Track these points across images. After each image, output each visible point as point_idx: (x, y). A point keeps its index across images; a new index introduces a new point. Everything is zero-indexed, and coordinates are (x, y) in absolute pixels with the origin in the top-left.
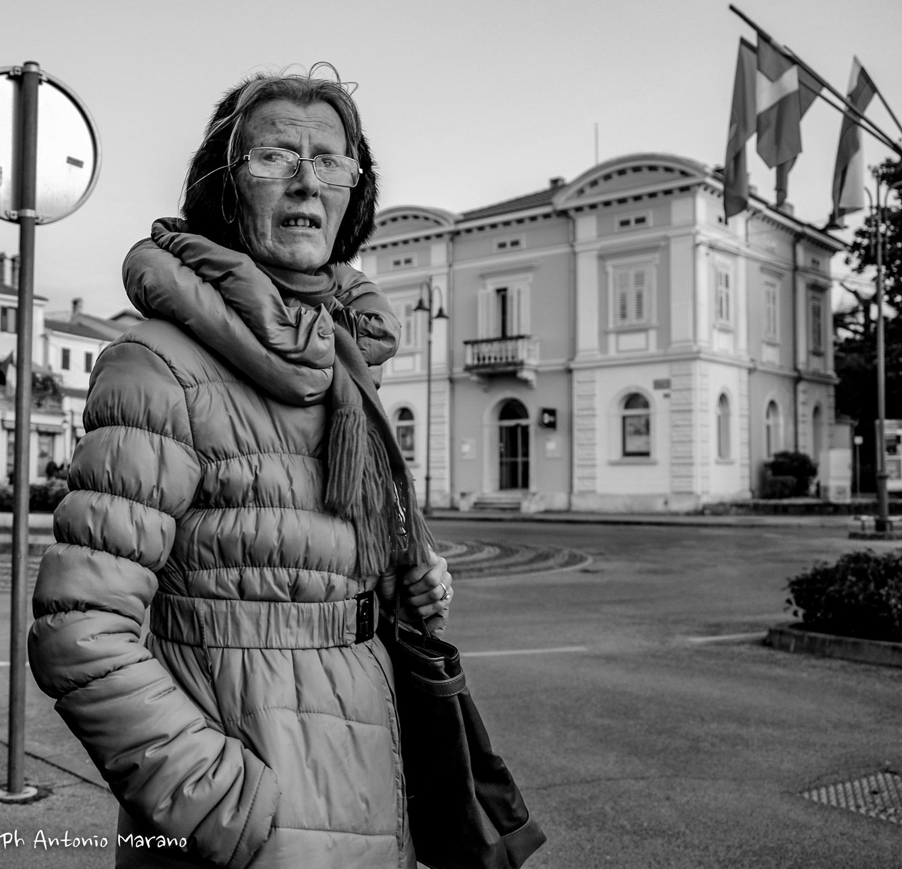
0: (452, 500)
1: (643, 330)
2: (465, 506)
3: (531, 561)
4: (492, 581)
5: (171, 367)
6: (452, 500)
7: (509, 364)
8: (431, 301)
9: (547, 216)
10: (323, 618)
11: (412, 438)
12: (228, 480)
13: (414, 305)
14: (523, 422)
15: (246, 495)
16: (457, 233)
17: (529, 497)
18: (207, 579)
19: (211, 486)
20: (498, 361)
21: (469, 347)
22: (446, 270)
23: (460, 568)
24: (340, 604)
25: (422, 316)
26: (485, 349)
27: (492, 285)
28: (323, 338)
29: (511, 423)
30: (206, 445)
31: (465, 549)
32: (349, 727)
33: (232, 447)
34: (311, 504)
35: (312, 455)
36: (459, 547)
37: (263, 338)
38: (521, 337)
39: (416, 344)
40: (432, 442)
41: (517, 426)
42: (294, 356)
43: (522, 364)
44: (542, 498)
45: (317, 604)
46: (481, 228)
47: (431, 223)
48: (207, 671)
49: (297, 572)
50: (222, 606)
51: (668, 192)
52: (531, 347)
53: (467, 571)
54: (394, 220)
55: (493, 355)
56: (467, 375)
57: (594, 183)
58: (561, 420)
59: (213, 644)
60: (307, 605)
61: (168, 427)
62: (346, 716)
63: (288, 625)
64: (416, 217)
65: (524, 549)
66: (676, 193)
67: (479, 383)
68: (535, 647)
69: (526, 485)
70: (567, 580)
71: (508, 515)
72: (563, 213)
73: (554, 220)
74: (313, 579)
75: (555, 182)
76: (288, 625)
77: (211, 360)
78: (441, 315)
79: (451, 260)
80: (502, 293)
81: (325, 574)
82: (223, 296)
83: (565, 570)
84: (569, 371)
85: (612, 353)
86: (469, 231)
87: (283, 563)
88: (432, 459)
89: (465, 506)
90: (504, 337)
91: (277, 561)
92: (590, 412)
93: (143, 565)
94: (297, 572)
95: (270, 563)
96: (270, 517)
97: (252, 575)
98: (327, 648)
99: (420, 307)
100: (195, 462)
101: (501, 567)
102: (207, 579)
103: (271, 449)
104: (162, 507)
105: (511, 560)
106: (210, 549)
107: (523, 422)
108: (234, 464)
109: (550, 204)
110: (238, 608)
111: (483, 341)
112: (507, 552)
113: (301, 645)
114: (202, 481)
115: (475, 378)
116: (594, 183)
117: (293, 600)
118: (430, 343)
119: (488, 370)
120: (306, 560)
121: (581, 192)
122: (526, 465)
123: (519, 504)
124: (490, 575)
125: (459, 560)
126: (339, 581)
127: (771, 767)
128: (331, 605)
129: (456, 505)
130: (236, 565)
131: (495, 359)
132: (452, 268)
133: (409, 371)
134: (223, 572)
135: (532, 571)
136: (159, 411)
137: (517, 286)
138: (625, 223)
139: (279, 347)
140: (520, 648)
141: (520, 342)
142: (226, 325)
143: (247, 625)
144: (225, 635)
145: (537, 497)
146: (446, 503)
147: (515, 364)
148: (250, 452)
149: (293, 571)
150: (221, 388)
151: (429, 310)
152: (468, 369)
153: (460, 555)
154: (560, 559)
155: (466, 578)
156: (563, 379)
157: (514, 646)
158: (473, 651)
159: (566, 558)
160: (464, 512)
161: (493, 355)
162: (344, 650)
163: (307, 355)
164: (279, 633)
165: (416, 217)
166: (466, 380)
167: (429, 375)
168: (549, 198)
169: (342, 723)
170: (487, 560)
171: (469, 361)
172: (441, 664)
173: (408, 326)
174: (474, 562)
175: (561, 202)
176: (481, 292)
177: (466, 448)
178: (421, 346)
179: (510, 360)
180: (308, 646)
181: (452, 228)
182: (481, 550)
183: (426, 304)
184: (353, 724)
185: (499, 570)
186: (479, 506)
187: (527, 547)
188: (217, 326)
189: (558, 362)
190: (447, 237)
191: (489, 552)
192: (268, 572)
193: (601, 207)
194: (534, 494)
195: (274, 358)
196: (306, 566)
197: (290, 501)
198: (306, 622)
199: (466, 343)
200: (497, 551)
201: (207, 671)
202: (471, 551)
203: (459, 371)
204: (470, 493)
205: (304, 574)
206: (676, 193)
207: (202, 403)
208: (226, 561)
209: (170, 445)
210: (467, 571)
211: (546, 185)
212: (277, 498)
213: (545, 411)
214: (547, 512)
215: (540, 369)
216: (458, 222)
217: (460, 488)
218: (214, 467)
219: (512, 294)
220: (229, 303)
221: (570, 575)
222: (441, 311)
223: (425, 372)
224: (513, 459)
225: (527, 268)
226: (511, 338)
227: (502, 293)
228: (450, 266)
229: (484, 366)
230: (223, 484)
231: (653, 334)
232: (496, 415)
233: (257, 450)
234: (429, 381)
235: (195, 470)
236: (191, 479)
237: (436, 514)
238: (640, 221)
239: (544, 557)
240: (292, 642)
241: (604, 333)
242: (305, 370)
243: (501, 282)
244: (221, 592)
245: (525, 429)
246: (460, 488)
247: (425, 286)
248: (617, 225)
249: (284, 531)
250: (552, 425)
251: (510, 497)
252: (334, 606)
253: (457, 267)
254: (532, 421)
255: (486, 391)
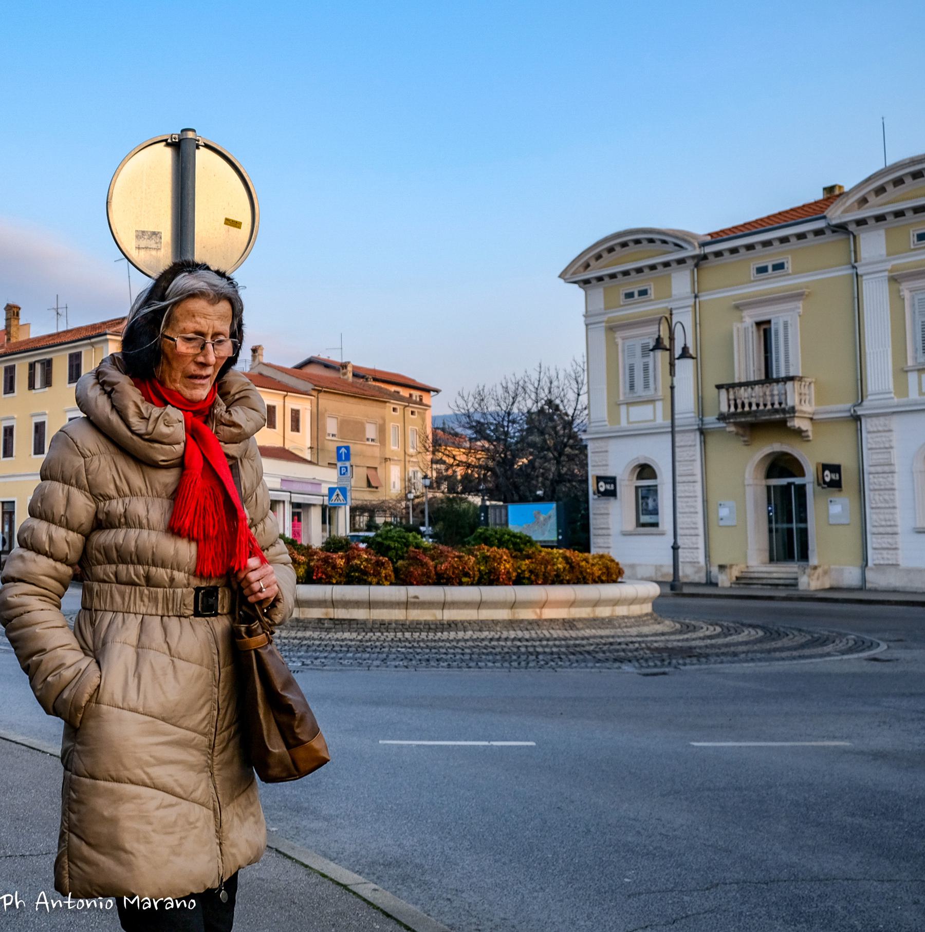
0: (708, 573)
1: (652, 401)
2: (724, 580)
3: (803, 646)
4: (748, 667)
5: (77, 446)
6: (708, 573)
7: (776, 411)
8: (672, 339)
9: (818, 233)
10: (166, 599)
11: (655, 500)
12: (109, 511)
13: (652, 344)
14: (798, 481)
15: (119, 520)
16: (705, 257)
17: (808, 571)
18: (99, 570)
19: (101, 516)
20: (761, 407)
21: (723, 392)
22: (691, 302)
23: (708, 651)
24: (179, 591)
25: (661, 357)
26: (744, 394)
27: (749, 318)
28: (168, 426)
29: (784, 481)
30: (96, 492)
31: (718, 629)
32: (173, 661)
33: (112, 491)
34: (162, 526)
35: (168, 498)
36: (711, 628)
37: (129, 426)
38: (792, 379)
39: (656, 389)
40: (678, 504)
41: (789, 484)
42: (147, 437)
43: (793, 410)
44: (825, 573)
45: (162, 589)
46: (734, 251)
47: (670, 247)
48: (92, 624)
49: (172, 572)
50: (106, 586)
51: (667, 264)
52: (805, 390)
53: (717, 655)
54: (624, 245)
55: (754, 401)
56: (722, 425)
57: (599, 257)
58: (848, 477)
59: (99, 608)
60: (155, 589)
61: (73, 481)
62: (171, 655)
63: (142, 600)
64: (651, 241)
65: (796, 633)
66: (674, 265)
67: (737, 434)
68: (787, 740)
69: (804, 556)
70: (847, 668)
71: (782, 593)
72: (841, 228)
73: (829, 237)
74: (161, 573)
75: (830, 190)
76: (142, 600)
77: (102, 438)
78: (685, 354)
79: (696, 291)
80: (764, 327)
81: (169, 571)
82: (112, 402)
83: (845, 657)
84: (857, 419)
85: (624, 423)
86: (718, 254)
87: (140, 563)
88: (679, 526)
89: (724, 580)
90: (768, 379)
91: (136, 561)
92: (690, 478)
93: (67, 565)
94: (172, 572)
95: (133, 563)
96: (133, 533)
97: (123, 568)
98: (169, 616)
99: (658, 345)
100: (90, 501)
101: (762, 652)
102: (99, 570)
103: (139, 494)
104: (68, 527)
105: (774, 645)
106: (100, 552)
107: (798, 481)
108: (114, 502)
109: (824, 217)
110: (113, 588)
111: (741, 385)
112: (772, 634)
113: (149, 612)
114: (96, 513)
115: (732, 429)
116: (599, 257)
117: (147, 586)
118: (672, 388)
119: (749, 419)
120: (153, 560)
121: (587, 266)
122: (804, 533)
123: (796, 579)
124: (747, 661)
125: (709, 642)
126: (180, 576)
127: (838, 821)
128: (171, 590)
129: (714, 580)
130: (114, 563)
131: (758, 405)
132: (697, 300)
133: (650, 421)
134: (108, 566)
135: (801, 657)
136: (69, 471)
137: (779, 316)
138: (762, 270)
139: (137, 432)
140: (765, 740)
141: (789, 385)
142: (108, 419)
143: (118, 598)
144: (105, 603)
145: (820, 570)
146: (701, 577)
147: (784, 411)
148: (125, 496)
149: (146, 567)
150: (109, 458)
151: (671, 350)
152: (722, 417)
153: (710, 637)
154: (841, 646)
155: (715, 663)
156: (849, 430)
157: (758, 738)
158: (705, 741)
159: (851, 643)
160: (724, 588)
161: (754, 401)
162: (182, 619)
163: (154, 436)
164: (135, 604)
165: (651, 241)
166: (721, 431)
167: (673, 426)
168: (823, 212)
169: (166, 659)
170: (746, 643)
171: (724, 409)
172: (243, 629)
173: (646, 368)
174: (727, 645)
175: (836, 214)
176: (736, 326)
177: (724, 512)
178: (662, 391)
179: (777, 406)
180: (154, 613)
181: (697, 252)
182: (737, 632)
183: (666, 343)
184: (175, 660)
185: (759, 655)
186: (742, 580)
187: (800, 630)
188: (103, 419)
189: (842, 407)
190: (691, 263)
191: (747, 634)
192: (131, 568)
193: (607, 279)
194: (815, 568)
195: (135, 437)
196: (155, 564)
197: (146, 525)
198: (154, 599)
199: (719, 387)
200: (761, 633)
201: (92, 624)
202: (726, 632)
203: (711, 420)
204: (731, 566)
205: (153, 569)
206: (674, 265)
207: (95, 465)
208: (110, 561)
209: (74, 491)
210: (717, 655)
211: (819, 195)
212: (138, 522)
213: (825, 467)
214: (832, 589)
215: (815, 417)
216: (704, 245)
217: (717, 560)
218: (102, 504)
219: (777, 326)
220: (113, 407)
221: (854, 662)
222: (685, 349)
223: (668, 422)
224: (789, 526)
225: (797, 296)
226: (777, 381)
227: (764, 327)
228: (696, 297)
229: (743, 414)
230: (106, 513)
231: (659, 405)
232: (763, 473)
233: (146, 494)
234: (673, 433)
235: (91, 507)
236: (88, 511)
237: (686, 590)
238: (643, 293)
239: (822, 641)
240: (143, 610)
241: (614, 405)
242: (156, 445)
243: (763, 313)
244: (106, 578)
245: (801, 489)
246: (717, 560)
247: (664, 320)
248: (753, 271)
249: (139, 542)
250: (836, 485)
251: (783, 570)
252: (174, 592)
253: (704, 298)
254: (809, 479)
255: (747, 444)
